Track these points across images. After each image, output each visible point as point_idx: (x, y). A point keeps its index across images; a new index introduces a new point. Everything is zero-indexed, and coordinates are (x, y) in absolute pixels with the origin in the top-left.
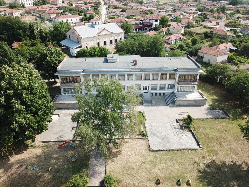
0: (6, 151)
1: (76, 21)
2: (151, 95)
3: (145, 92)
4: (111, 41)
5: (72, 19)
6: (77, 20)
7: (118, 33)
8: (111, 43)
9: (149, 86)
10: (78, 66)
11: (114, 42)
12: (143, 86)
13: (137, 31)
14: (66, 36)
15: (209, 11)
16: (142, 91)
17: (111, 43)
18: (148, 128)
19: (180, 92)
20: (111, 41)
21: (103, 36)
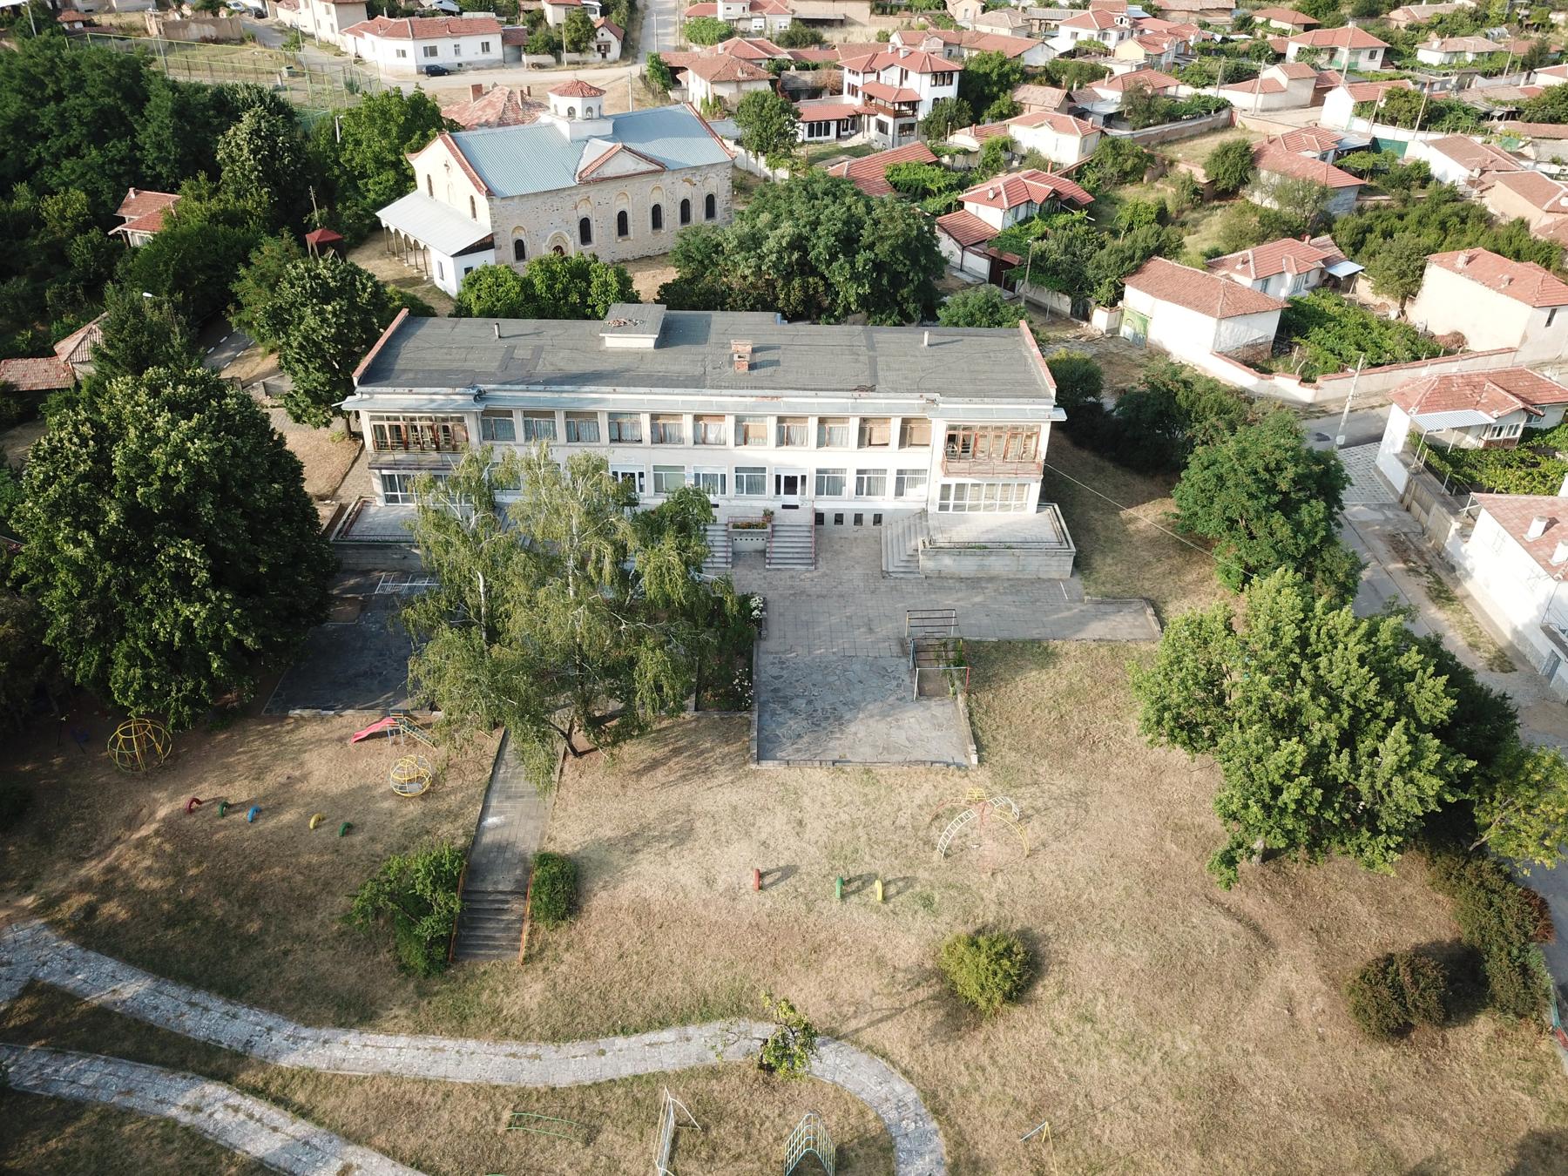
0: (128, 743)
1: (487, 56)
2: (811, 519)
3: (784, 507)
4: (657, 210)
5: (456, 41)
6: (486, 47)
7: (697, 168)
8: (657, 221)
9: (778, 492)
10: (455, 365)
11: (671, 215)
12: (778, 477)
13: (827, 133)
14: (412, 178)
15: (489, 588)
16: (769, 500)
17: (657, 221)
18: (1538, 497)
19: (955, 507)
20: (657, 210)
21: (612, 184)
